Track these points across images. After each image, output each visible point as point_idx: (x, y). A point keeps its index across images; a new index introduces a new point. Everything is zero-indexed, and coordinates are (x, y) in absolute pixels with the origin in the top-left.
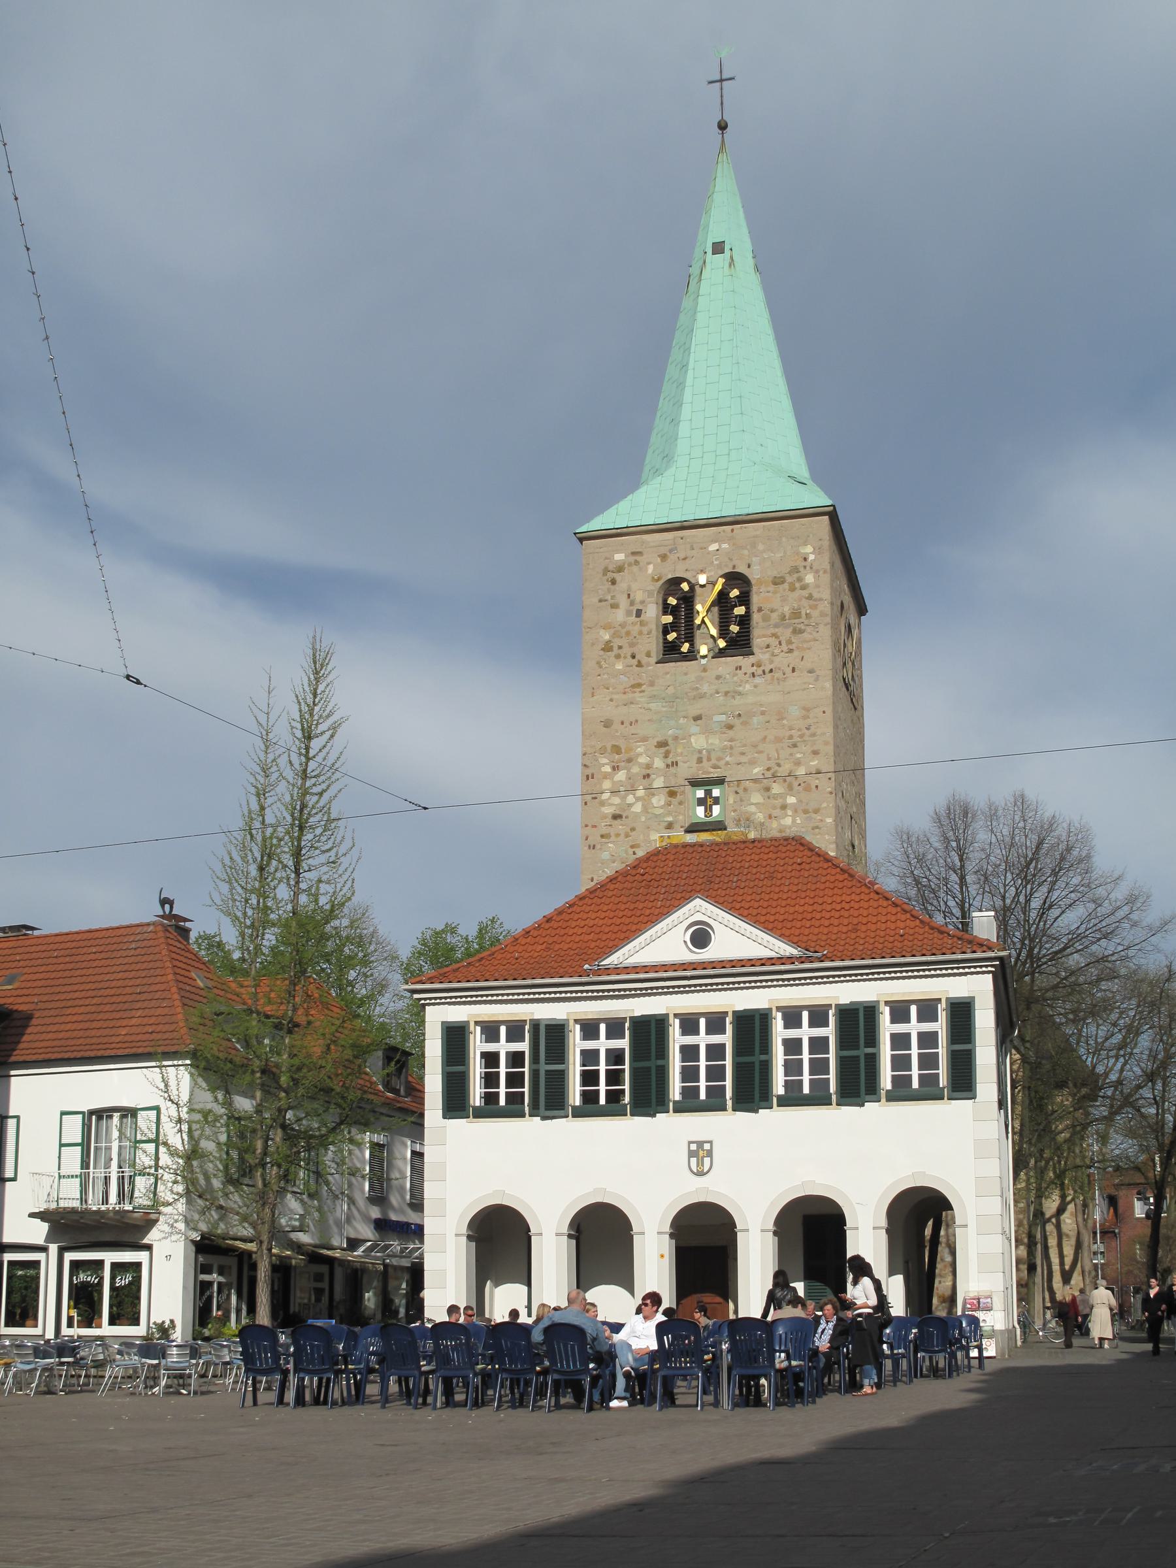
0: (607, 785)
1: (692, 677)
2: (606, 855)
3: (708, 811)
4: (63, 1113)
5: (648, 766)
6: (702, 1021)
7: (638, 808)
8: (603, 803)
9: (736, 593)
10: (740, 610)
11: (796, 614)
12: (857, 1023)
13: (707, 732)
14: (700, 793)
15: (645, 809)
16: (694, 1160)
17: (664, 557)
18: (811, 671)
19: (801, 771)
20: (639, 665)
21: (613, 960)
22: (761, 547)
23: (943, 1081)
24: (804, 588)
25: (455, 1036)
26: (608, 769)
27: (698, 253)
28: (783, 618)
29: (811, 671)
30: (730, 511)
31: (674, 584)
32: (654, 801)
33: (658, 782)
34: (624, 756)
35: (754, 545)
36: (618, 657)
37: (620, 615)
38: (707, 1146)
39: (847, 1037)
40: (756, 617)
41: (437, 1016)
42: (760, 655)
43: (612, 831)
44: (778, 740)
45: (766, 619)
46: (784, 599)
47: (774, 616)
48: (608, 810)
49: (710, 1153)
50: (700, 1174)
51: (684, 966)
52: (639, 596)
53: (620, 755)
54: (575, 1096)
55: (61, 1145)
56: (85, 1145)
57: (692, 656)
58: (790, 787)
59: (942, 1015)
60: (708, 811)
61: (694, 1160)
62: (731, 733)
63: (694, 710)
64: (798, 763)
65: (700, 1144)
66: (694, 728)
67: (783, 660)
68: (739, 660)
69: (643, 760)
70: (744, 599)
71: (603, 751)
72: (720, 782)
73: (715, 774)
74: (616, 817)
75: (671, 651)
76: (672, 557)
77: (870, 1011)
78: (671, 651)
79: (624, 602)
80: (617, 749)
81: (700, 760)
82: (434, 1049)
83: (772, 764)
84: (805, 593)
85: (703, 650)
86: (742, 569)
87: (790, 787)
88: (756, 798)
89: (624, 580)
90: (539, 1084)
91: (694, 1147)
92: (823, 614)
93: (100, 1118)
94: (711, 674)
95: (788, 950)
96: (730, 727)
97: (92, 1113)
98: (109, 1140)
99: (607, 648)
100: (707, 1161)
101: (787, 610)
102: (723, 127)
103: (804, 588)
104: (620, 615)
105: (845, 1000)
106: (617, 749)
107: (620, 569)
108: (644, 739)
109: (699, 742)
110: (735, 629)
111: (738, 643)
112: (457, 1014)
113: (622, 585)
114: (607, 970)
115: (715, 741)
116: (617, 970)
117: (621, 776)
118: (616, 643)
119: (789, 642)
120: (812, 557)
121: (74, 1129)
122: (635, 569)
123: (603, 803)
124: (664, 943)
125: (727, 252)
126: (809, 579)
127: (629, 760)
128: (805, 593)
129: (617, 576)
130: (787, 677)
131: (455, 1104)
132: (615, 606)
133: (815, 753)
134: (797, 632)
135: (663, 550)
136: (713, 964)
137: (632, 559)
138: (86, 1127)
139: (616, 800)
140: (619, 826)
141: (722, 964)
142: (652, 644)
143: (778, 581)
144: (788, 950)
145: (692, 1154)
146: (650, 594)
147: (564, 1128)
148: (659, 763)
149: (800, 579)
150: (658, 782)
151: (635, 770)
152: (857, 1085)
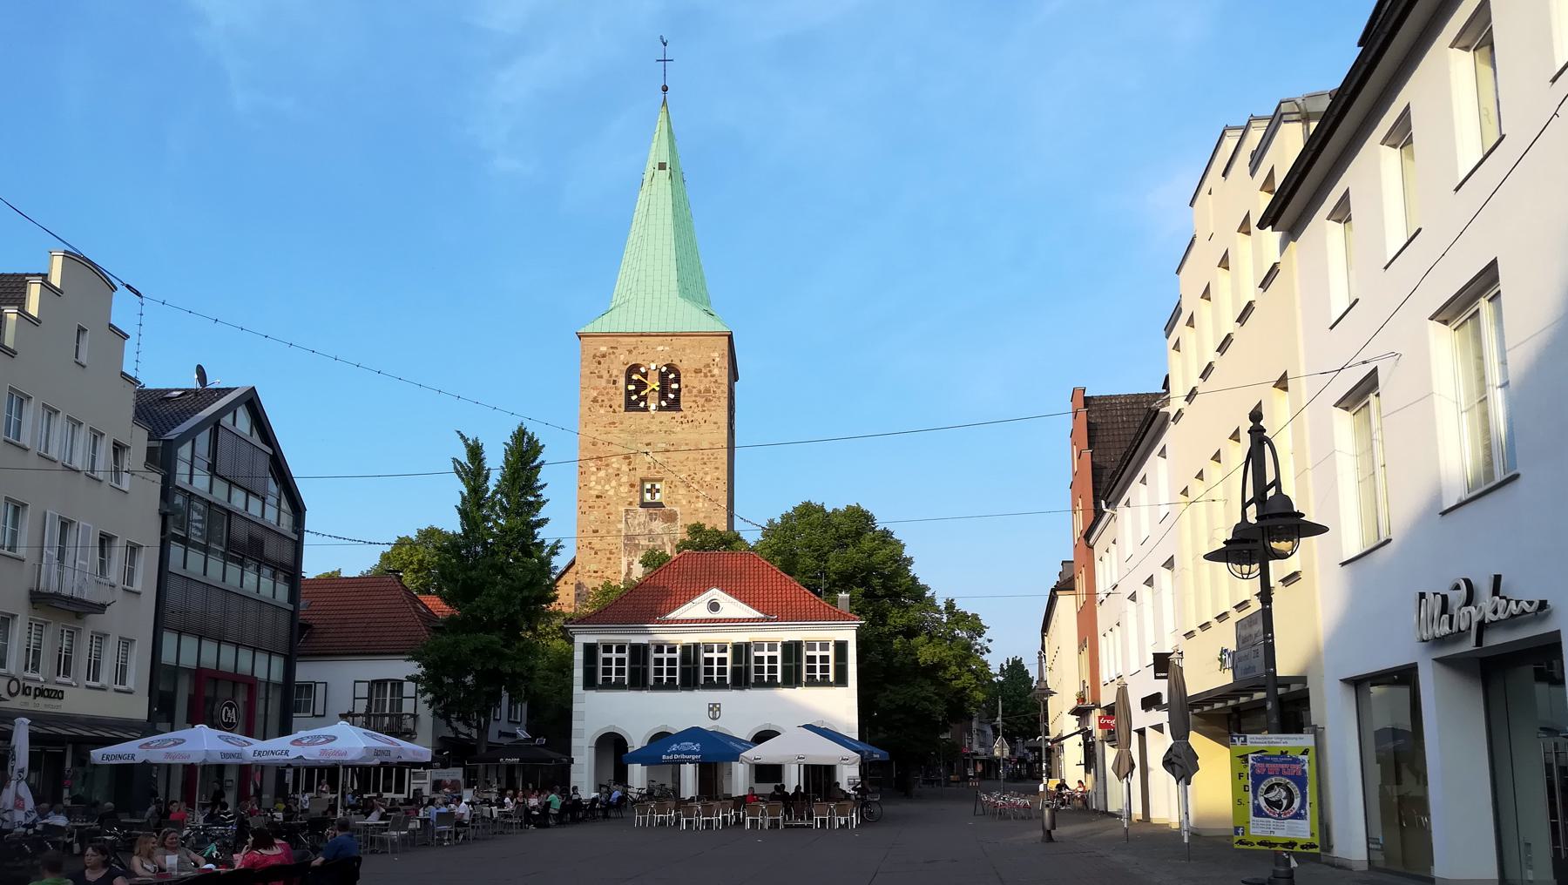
0: (593, 478)
3: (653, 496)
7: (611, 492)
9: (670, 375)
10: (675, 386)
11: (707, 390)
12: (792, 650)
15: (616, 494)
19: (708, 478)
21: (671, 616)
23: (832, 679)
25: (590, 650)
27: (649, 167)
31: (634, 368)
33: (624, 479)
37: (603, 382)
40: (684, 391)
41: (581, 640)
42: (686, 412)
50: (714, 719)
51: (706, 621)
52: (615, 373)
54: (651, 682)
56: (370, 698)
57: (646, 409)
60: (653, 496)
67: (699, 416)
68: (673, 413)
70: (677, 380)
72: (660, 480)
75: (631, 406)
77: (798, 644)
78: (631, 406)
79: (606, 375)
82: (579, 656)
85: (653, 406)
86: (676, 362)
88: (682, 491)
90: (640, 672)
95: (759, 615)
99: (595, 400)
102: (665, 89)
106: (599, 458)
110: (671, 396)
111: (674, 405)
112: (592, 639)
114: (668, 621)
116: (673, 621)
117: (602, 474)
121: (363, 690)
124: (696, 609)
126: (716, 371)
130: (699, 425)
131: (590, 683)
136: (720, 620)
142: (621, 400)
143: (697, 371)
144: (759, 615)
147: (645, 694)
148: (625, 468)
150: (624, 479)
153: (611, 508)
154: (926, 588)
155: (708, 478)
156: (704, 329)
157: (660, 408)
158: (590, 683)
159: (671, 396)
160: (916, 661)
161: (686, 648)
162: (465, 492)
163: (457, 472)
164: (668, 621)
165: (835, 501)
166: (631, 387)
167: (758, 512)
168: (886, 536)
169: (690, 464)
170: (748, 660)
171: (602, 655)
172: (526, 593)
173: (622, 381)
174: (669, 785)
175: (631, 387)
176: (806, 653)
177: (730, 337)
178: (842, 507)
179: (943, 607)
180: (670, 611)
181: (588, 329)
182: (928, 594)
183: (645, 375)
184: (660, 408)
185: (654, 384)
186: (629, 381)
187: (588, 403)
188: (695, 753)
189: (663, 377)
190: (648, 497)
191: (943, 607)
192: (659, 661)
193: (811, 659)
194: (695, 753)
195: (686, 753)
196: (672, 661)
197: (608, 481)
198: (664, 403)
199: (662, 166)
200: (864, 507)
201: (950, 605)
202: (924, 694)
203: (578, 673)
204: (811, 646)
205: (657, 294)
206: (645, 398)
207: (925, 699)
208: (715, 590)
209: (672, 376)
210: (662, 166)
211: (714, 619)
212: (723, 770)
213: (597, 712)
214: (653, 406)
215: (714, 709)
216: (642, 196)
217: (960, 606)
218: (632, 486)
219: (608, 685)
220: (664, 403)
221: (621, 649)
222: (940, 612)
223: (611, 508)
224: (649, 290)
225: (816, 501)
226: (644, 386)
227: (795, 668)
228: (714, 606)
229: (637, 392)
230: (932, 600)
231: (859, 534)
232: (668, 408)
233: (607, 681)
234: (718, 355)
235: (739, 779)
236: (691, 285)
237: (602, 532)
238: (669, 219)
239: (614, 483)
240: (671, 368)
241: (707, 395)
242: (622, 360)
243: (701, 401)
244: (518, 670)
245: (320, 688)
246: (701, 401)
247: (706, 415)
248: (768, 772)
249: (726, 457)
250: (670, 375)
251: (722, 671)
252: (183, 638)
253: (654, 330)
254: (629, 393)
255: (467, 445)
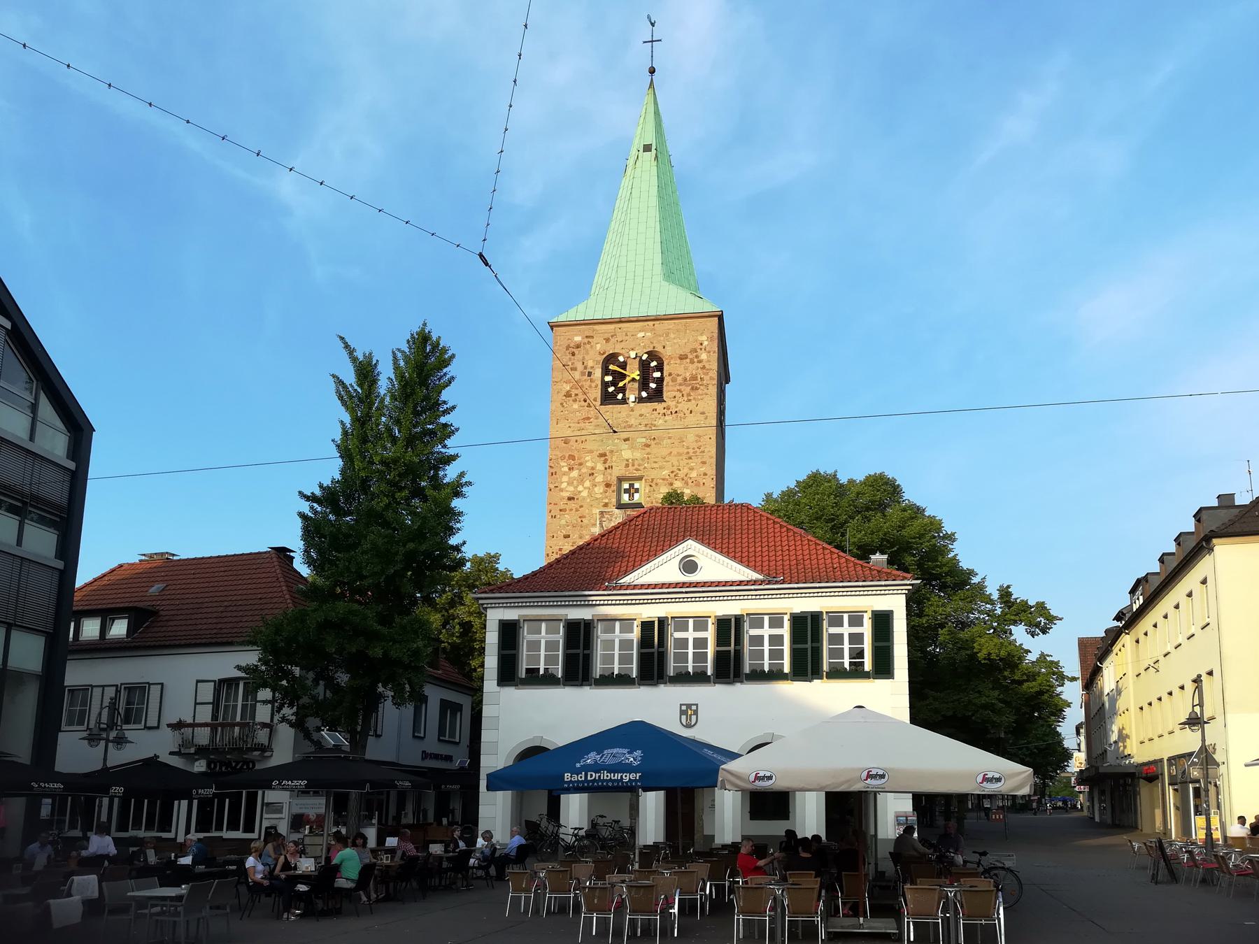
0: (565, 479)
1: (624, 414)
2: (563, 522)
3: (626, 491)
4: (198, 681)
5: (593, 468)
6: (766, 618)
7: (585, 494)
8: (562, 490)
9: (651, 365)
10: (657, 375)
11: (694, 378)
12: (807, 628)
13: (632, 448)
14: (626, 486)
15: (590, 495)
16: (684, 717)
17: (607, 340)
18: (703, 413)
20: (589, 406)
21: (627, 580)
22: (672, 336)
23: (868, 666)
24: (700, 362)
25: (509, 631)
26: (566, 469)
27: (634, 152)
28: (685, 380)
29: (703, 413)
30: (652, 312)
31: (611, 358)
32: (596, 489)
33: (599, 478)
34: (577, 462)
35: (667, 335)
36: (575, 401)
37: (577, 375)
38: (694, 708)
39: (797, 636)
41: (495, 616)
43: (567, 507)
44: (679, 454)
45: (674, 380)
46: (686, 369)
47: (680, 379)
48: (566, 495)
49: (696, 713)
52: (590, 363)
53: (574, 461)
55: (196, 704)
56: (216, 704)
57: (624, 401)
58: (687, 483)
59: (787, 624)
60: (631, 497)
61: (684, 717)
62: (648, 450)
63: (625, 435)
64: (692, 469)
65: (689, 706)
66: (625, 446)
67: (684, 406)
68: (655, 405)
69: (589, 464)
70: (660, 368)
71: (563, 458)
72: (640, 479)
73: (638, 474)
74: (570, 499)
75: (608, 398)
76: (613, 340)
77: (816, 617)
78: (608, 398)
79: (580, 367)
80: (572, 457)
81: (627, 466)
82: (492, 638)
83: (675, 469)
84: (700, 365)
85: (632, 398)
86: (659, 349)
87: (687, 483)
89: (580, 354)
91: (684, 708)
92: (711, 378)
93: (229, 687)
94: (637, 413)
95: (755, 576)
96: (648, 446)
97: (222, 681)
98: (236, 700)
99: (568, 395)
100: (694, 718)
101: (688, 375)
102: (652, 71)
103: (700, 362)
104: (577, 375)
105: (797, 610)
106: (572, 457)
107: (578, 346)
108: (591, 452)
109: (627, 454)
110: (653, 385)
111: (657, 396)
112: (511, 615)
113: (579, 356)
114: (621, 587)
115: (638, 455)
116: (628, 587)
117: (575, 474)
118: (574, 392)
119: (689, 395)
120: (706, 343)
121: (207, 693)
122: (588, 346)
123: (562, 490)
124: (664, 569)
125: (654, 151)
126: (704, 356)
127: (581, 464)
128: (700, 365)
129: (576, 351)
130: (688, 412)
132: (574, 369)
133: (704, 463)
134: (694, 389)
135: (606, 336)
136: (697, 584)
137: (586, 340)
138: (217, 692)
139: (571, 489)
140: (572, 504)
141: (704, 584)
142: (596, 393)
143: (683, 357)
144: (755, 576)
145: (682, 713)
146: (598, 362)
148: (600, 467)
149: (697, 357)
150: (599, 478)
151: (584, 470)
152: (807, 665)
153: (585, 511)
154: (971, 573)
155: (694, 474)
156: (689, 309)
157: (640, 400)
158: (508, 676)
159: (653, 385)
160: (973, 657)
161: (647, 626)
162: (347, 419)
163: (341, 398)
164: (621, 587)
165: (852, 469)
166: (608, 378)
167: (756, 479)
168: (917, 511)
169: (674, 460)
170: (739, 640)
172: (411, 546)
173: (598, 373)
174: (626, 823)
175: (608, 378)
176: (828, 630)
177: (721, 318)
178: (860, 477)
179: (995, 596)
180: (626, 573)
181: (562, 318)
182: (975, 580)
183: (624, 366)
184: (640, 400)
185: (634, 373)
186: (606, 371)
187: (561, 396)
188: (628, 768)
189: (644, 366)
190: (625, 498)
191: (995, 596)
193: (837, 639)
194: (628, 768)
195: (612, 769)
196: (625, 644)
197: (582, 482)
198: (644, 394)
199: (647, 148)
200: (890, 474)
201: (1005, 594)
202: (983, 700)
203: (491, 662)
204: (836, 620)
205: (639, 279)
206: (623, 390)
207: (985, 707)
209: (654, 364)
210: (647, 148)
211: (689, 586)
212: (701, 800)
213: (520, 719)
214: (632, 398)
215: (689, 712)
216: (625, 182)
217: (1018, 594)
218: (608, 485)
219: (535, 679)
220: (644, 394)
222: (992, 602)
223: (585, 511)
224: (630, 276)
225: (826, 468)
226: (623, 376)
227: (808, 652)
228: (689, 566)
229: (614, 383)
230: (981, 587)
231: (881, 507)
232: (649, 399)
234: (706, 336)
235: (727, 819)
236: (676, 266)
238: (654, 201)
240: (652, 355)
241: (693, 384)
242: (600, 348)
243: (687, 390)
244: (393, 654)
245: (155, 691)
246: (687, 390)
247: (691, 405)
248: (769, 803)
249: (714, 450)
250: (651, 365)
251: (701, 657)
252: (15, 634)
253: (634, 314)
254: (605, 385)
255: (354, 360)
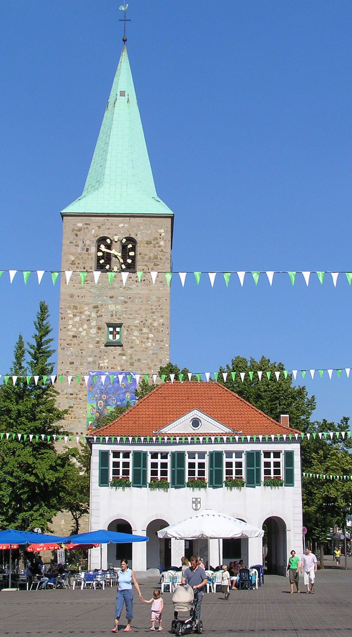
0: (71, 322)
3: (114, 337)
7: (84, 333)
11: (156, 257)
12: (253, 457)
19: (155, 324)
25: (104, 456)
33: (94, 323)
37: (79, 250)
40: (138, 258)
52: (88, 242)
60: (114, 337)
79: (81, 244)
86: (133, 236)
88: (136, 333)
106: (75, 308)
117: (77, 319)
124: (181, 426)
126: (162, 243)
131: (104, 481)
142: (93, 264)
143: (148, 243)
148: (94, 315)
150: (94, 323)
153: (84, 346)
155: (155, 324)
158: (104, 481)
159: (129, 261)
171: (112, 459)
173: (93, 249)
180: (163, 426)
189: (124, 247)
192: (267, 464)
193: (229, 465)
197: (82, 325)
198: (108, 267)
208: (196, 411)
214: (116, 269)
218: (99, 329)
221: (126, 455)
223: (84, 346)
227: (253, 473)
233: (229, 479)
237: (77, 364)
239: (85, 327)
